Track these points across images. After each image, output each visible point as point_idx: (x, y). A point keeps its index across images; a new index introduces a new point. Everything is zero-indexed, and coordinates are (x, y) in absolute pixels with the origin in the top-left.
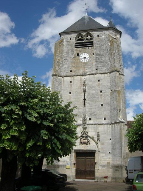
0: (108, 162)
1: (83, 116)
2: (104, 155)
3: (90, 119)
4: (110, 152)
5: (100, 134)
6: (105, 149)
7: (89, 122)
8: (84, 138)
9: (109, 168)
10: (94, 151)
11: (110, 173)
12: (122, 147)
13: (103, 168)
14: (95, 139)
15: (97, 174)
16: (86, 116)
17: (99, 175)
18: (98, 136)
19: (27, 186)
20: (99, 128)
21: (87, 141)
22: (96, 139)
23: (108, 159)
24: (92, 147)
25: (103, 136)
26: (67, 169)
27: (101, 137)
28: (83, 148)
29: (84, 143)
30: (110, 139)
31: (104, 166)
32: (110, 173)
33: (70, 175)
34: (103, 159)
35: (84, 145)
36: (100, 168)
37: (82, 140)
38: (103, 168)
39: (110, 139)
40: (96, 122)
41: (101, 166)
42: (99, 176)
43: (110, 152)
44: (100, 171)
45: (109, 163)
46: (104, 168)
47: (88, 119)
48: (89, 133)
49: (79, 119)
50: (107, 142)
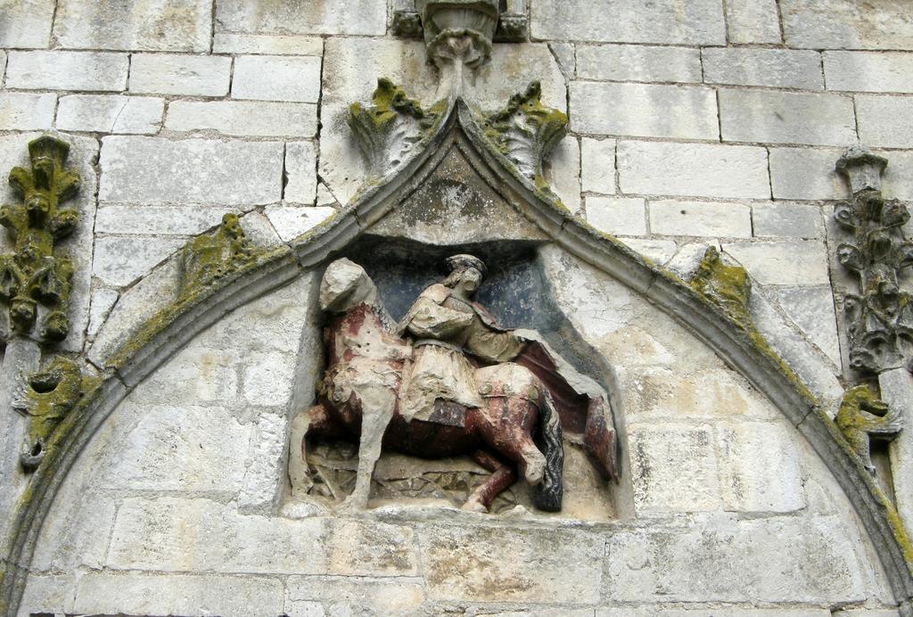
8: (434, 304)
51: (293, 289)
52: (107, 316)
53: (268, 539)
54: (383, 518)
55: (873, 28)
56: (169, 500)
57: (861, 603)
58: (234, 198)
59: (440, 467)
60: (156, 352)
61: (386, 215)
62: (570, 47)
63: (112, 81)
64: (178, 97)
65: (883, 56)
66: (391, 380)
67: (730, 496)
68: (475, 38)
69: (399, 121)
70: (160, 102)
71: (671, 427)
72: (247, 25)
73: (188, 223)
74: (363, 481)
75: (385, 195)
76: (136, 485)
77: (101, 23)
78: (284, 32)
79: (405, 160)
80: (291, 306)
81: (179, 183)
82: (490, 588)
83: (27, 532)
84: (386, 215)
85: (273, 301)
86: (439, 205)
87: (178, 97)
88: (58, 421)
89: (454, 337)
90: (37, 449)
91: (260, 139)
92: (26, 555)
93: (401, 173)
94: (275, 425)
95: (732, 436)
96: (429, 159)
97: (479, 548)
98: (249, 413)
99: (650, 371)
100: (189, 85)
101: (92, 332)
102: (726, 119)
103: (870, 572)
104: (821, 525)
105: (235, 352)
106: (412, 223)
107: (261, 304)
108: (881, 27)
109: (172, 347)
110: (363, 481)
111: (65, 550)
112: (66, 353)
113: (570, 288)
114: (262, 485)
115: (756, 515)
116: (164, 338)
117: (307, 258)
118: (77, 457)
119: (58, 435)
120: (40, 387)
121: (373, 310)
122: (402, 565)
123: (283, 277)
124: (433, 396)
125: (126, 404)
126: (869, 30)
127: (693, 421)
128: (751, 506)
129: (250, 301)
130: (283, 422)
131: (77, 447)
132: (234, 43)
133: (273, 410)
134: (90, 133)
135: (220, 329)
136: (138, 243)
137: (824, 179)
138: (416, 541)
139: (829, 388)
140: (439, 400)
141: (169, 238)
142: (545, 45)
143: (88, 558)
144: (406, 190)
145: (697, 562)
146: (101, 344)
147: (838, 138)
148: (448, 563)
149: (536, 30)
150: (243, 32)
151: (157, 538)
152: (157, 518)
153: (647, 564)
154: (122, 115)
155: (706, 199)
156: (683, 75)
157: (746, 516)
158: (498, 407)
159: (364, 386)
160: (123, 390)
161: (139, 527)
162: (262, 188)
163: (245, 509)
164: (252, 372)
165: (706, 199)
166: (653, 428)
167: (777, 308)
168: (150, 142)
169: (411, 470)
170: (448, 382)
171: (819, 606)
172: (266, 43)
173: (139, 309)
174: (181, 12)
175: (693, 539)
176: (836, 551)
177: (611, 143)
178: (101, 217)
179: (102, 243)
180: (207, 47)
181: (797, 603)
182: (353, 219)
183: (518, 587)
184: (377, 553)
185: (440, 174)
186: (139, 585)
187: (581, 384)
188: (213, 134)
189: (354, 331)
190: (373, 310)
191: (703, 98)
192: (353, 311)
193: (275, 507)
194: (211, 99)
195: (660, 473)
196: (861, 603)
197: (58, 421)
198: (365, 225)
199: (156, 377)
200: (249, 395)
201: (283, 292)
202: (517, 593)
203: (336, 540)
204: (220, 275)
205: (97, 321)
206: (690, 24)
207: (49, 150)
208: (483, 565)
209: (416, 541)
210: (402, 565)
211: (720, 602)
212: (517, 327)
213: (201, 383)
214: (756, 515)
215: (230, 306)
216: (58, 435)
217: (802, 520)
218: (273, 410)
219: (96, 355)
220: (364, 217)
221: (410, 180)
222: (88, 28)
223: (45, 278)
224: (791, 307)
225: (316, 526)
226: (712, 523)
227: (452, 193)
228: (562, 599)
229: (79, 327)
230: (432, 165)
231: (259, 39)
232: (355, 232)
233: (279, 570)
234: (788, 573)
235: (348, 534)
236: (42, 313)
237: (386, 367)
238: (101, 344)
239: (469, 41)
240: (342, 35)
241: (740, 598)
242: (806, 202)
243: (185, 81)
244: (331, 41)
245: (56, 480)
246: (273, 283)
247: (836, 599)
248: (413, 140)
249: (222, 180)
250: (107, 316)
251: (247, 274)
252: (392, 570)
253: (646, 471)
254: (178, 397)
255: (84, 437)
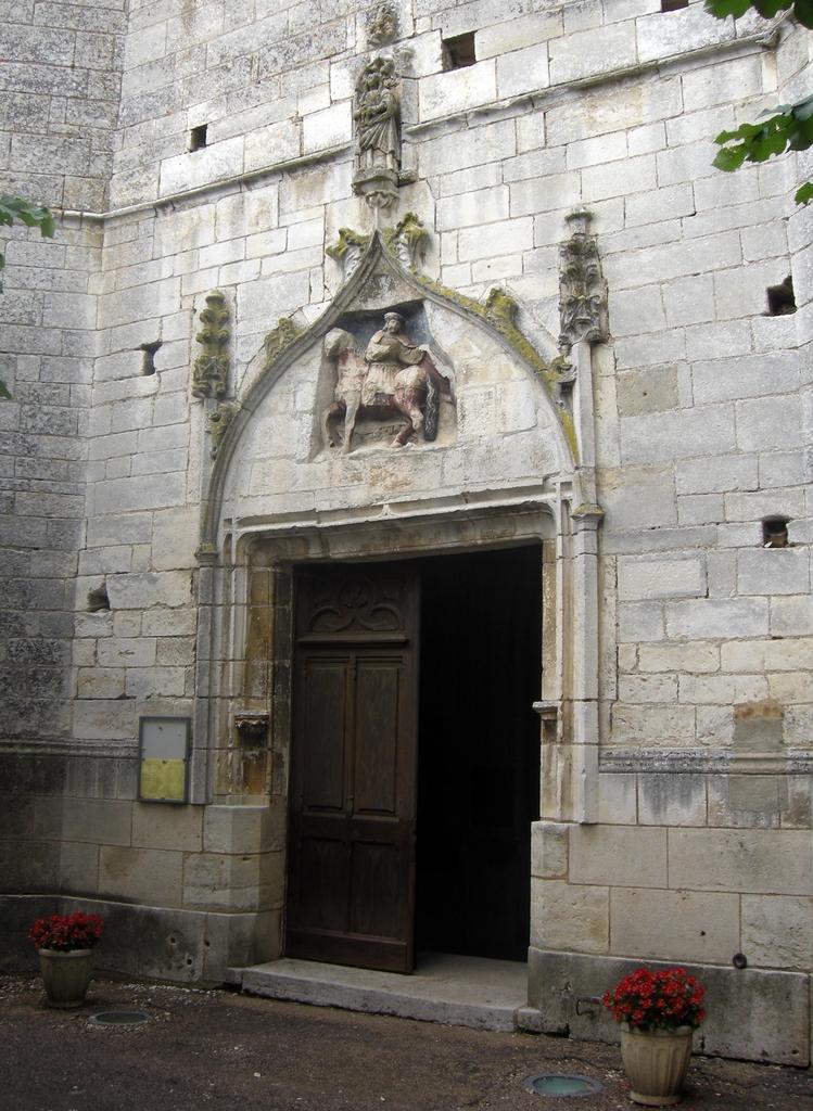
0: (751, 691)
1: (357, 37)
2: (682, 574)
3: (459, 53)
4: (775, 529)
5: (604, 231)
6: (687, 481)
7: (439, 92)
8: (376, 344)
9: (777, 807)
10: (522, 532)
11: (772, 909)
12: (260, 992)
13: (658, 806)
14: (528, 324)
15: (559, 910)
16: (406, 28)
17: (595, 932)
18: (581, 261)
19: (673, 10)
20: (595, 151)
21: (409, 376)
22: (544, 326)
23: (739, 655)
24: (489, 457)
25: (646, 256)
26: (147, 803)
27: (627, 275)
28: (358, 496)
29: (380, 413)
30: (781, 300)
31: (676, 774)
32: (772, 909)
33: (190, 894)
34: (666, 642)
35: (380, 448)
36: (621, 803)
37: (352, 368)
38: (658, 806)
39: (781, 300)
40: (539, 77)
41: (628, 766)
42: (589, 944)
43: (775, 529)
44: (610, 866)
45: (756, 719)
46: (679, 813)
47: (428, 54)
48: (444, 244)
49: (313, 88)
50: (723, 343)
51: (315, 348)
52: (243, 377)
53: (308, 474)
54: (351, 458)
55: (595, 121)
56: (271, 461)
57: (558, 474)
58: (290, 306)
59: (387, 424)
60: (259, 394)
61: (352, 301)
62: (437, 179)
63: (238, 255)
64: (266, 256)
65: (599, 138)
66: (358, 387)
67: (500, 425)
68: (382, 193)
69: (350, 250)
70: (259, 260)
71: (476, 391)
72: (292, 208)
73: (271, 324)
74: (346, 440)
75: (346, 292)
76: (258, 457)
77: (234, 224)
78: (308, 207)
79: (353, 272)
80: (313, 358)
81: (267, 303)
82: (394, 486)
83: (217, 485)
84: (352, 301)
85: (306, 357)
86: (379, 288)
87: (266, 256)
88: (223, 433)
89: (382, 359)
90: (215, 449)
91: (299, 271)
92: (219, 495)
93: (352, 279)
94: (308, 419)
95: (504, 392)
96: (367, 267)
97: (390, 467)
98: (297, 415)
99: (470, 361)
100: (271, 248)
101: (238, 386)
102: (513, 203)
103: (563, 456)
104: (542, 434)
105: (292, 386)
106: (365, 301)
107: (301, 360)
108: (599, 120)
109: (265, 390)
110: (346, 440)
111: (234, 490)
112: (230, 399)
113: (435, 322)
114: (303, 450)
115: (512, 433)
116: (260, 386)
117: (318, 332)
118: (235, 447)
119: (223, 440)
120: (216, 419)
121: (352, 351)
122: (360, 479)
123: (309, 344)
124: (374, 393)
125: (253, 419)
126: (592, 123)
127: (485, 386)
128: (509, 429)
129: (296, 359)
130: (311, 417)
131: (233, 444)
132: (287, 220)
133: (306, 412)
134: (232, 285)
135: (286, 376)
136: (253, 338)
137: (561, 229)
138: (365, 467)
139: (552, 352)
140: (377, 394)
141: (264, 333)
142: (424, 181)
143: (244, 493)
144: (359, 285)
145: (483, 462)
146: (242, 390)
147: (570, 202)
148: (378, 476)
149: (422, 173)
150: (291, 212)
151: (267, 479)
152: (266, 470)
153: (461, 465)
154: (247, 271)
155: (501, 256)
156: (492, 181)
157: (506, 434)
158: (401, 393)
159: (346, 392)
160: (249, 414)
161: (261, 475)
162: (300, 298)
163: (299, 462)
164: (299, 394)
165: (501, 256)
166: (468, 393)
167: (531, 314)
168: (255, 284)
169: (374, 427)
170: (379, 385)
171: (537, 477)
172: (301, 216)
173: (255, 371)
174: (265, 208)
175: (481, 450)
176: (548, 447)
177: (455, 233)
178: (238, 329)
179: (240, 341)
180: (276, 224)
181: (527, 477)
182: (334, 308)
183: (406, 484)
184: (349, 474)
185: (376, 272)
186: (261, 501)
187: (444, 371)
188: (281, 273)
189: (344, 364)
190: (352, 351)
191: (502, 193)
192: (342, 353)
193: (311, 458)
194: (279, 254)
195: (470, 417)
196: (558, 474)
197: (223, 433)
198: (342, 309)
199: (264, 404)
200: (298, 405)
201: (310, 351)
202: (405, 487)
203: (334, 471)
204: (288, 345)
205: (240, 380)
206: (497, 147)
207: (217, 301)
208: (392, 475)
209: (365, 467)
210: (360, 479)
211: (492, 481)
212: (419, 345)
213: (280, 404)
214: (512, 433)
215: (287, 364)
216: (223, 440)
217: (533, 432)
218: (306, 412)
219: (240, 398)
220: (340, 305)
221: (360, 280)
222: (229, 228)
223: (212, 368)
224: (538, 312)
225: (325, 465)
226: (491, 440)
227: (383, 279)
228: (423, 488)
229: (233, 386)
230: (371, 268)
231: (297, 214)
232: (338, 313)
233: (312, 488)
234: (524, 462)
235: (338, 467)
236: (214, 383)
237: (357, 380)
238: (242, 390)
239: (379, 195)
240: (333, 202)
241: (501, 477)
242: (552, 245)
243: (268, 246)
244: (328, 206)
245: (227, 460)
246: (305, 348)
247: (545, 473)
248: (357, 259)
249: (284, 297)
250: (243, 377)
251: (289, 348)
252: (356, 482)
253: (463, 417)
254: (270, 413)
255: (236, 438)
